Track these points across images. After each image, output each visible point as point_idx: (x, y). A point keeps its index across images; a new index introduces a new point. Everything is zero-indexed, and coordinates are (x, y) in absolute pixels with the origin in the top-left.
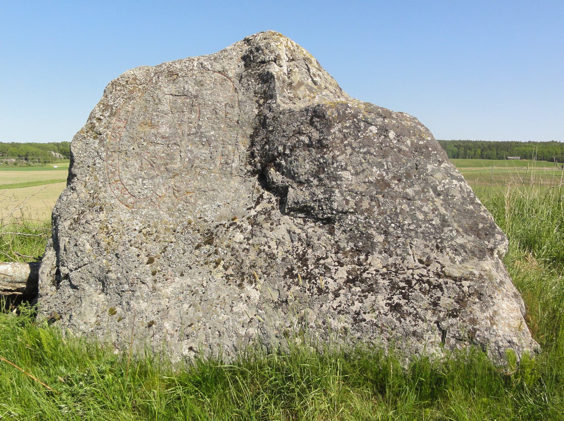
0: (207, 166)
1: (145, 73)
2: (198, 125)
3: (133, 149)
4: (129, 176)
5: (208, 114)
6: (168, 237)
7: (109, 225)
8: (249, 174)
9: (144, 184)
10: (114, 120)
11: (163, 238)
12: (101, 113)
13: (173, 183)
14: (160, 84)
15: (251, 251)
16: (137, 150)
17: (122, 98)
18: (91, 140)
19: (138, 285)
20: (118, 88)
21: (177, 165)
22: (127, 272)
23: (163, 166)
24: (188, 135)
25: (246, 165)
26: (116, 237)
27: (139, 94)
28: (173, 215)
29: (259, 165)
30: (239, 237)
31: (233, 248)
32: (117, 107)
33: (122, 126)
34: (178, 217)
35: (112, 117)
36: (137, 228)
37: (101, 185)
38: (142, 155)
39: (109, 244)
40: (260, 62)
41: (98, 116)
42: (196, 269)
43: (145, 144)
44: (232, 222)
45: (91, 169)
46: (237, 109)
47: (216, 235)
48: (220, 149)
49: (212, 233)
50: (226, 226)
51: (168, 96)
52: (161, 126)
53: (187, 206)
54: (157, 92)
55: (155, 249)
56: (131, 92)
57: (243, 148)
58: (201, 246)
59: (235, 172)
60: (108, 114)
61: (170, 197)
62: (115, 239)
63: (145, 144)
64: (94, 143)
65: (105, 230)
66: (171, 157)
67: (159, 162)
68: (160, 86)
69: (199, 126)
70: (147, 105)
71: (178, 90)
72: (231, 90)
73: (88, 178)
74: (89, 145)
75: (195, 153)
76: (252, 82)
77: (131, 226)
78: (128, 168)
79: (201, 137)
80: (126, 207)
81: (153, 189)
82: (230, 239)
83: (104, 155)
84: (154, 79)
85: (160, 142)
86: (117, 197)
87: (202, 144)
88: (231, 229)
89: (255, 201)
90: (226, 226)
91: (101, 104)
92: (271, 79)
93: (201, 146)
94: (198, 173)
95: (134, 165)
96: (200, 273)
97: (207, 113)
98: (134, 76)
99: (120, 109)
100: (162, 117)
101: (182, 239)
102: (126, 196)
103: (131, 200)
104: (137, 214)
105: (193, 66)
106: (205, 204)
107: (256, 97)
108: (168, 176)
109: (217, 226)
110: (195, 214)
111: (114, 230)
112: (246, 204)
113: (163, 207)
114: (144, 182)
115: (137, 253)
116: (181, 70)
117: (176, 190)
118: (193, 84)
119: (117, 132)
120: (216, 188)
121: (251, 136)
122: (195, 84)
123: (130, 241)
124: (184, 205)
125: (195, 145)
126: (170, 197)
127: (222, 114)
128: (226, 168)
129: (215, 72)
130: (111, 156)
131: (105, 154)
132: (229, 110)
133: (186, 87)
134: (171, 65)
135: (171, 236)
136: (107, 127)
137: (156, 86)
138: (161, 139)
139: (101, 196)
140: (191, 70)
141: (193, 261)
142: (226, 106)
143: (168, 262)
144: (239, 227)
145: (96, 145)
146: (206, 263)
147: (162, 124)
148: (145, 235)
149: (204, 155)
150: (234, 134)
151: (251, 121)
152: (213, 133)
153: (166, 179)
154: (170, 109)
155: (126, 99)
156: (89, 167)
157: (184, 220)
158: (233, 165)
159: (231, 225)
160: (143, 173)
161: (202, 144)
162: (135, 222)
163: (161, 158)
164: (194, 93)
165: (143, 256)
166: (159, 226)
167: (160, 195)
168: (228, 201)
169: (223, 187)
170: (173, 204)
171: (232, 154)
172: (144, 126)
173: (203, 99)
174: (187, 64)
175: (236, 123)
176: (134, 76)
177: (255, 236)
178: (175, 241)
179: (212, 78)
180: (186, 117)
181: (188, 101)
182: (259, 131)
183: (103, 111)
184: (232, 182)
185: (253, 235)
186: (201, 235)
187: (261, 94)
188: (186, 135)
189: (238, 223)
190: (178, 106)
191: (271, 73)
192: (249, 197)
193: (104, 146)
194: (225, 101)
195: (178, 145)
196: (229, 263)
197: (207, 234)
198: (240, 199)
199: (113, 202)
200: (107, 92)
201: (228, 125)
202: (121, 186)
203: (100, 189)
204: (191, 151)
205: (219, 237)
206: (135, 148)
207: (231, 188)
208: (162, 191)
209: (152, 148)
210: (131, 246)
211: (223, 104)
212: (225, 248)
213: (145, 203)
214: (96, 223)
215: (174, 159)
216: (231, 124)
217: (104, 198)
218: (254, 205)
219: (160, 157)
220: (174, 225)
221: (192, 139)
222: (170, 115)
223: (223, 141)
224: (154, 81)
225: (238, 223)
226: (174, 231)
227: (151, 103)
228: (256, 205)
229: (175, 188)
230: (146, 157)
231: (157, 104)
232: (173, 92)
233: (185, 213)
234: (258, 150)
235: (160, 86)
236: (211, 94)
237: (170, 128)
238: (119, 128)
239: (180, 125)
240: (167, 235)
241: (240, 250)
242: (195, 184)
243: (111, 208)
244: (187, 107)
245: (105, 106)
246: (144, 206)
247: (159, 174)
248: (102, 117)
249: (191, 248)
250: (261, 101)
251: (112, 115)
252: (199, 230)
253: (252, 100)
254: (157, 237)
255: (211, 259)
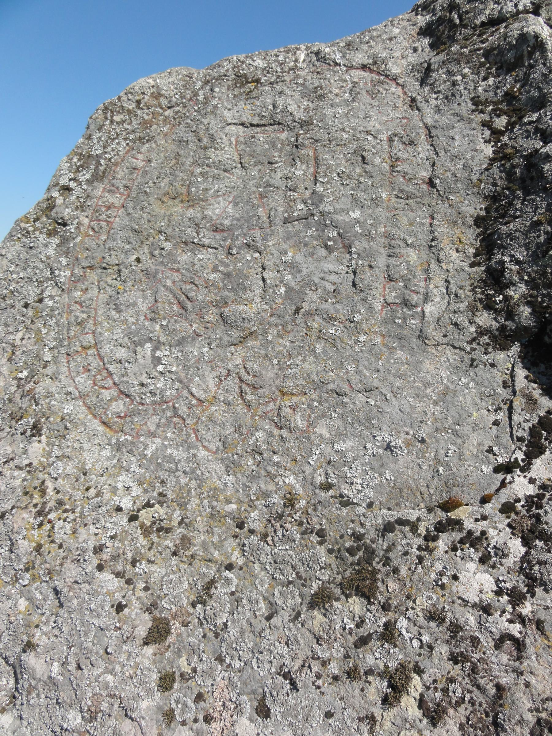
0: (343, 311)
1: (182, 83)
2: (314, 193)
3: (138, 260)
4: (118, 333)
5: (340, 165)
6: (219, 546)
7: (50, 485)
8: (486, 339)
9: (157, 361)
10: (99, 189)
11: (204, 546)
12: (72, 175)
13: (239, 361)
14: (214, 102)
15: (531, 650)
16: (148, 263)
17: (125, 139)
18: (42, 238)
19: (111, 722)
20: (117, 118)
21: (252, 307)
22: (79, 668)
23: (214, 310)
24: (286, 221)
25: (473, 309)
26: (63, 530)
27: (165, 129)
28: (238, 465)
29: (526, 311)
30: (477, 581)
31: (455, 628)
32: (110, 159)
33: (117, 203)
34: (253, 477)
35: (96, 184)
36: (126, 504)
37: (48, 357)
38: (160, 276)
39: (38, 548)
40: (483, 24)
41: (63, 181)
42: (314, 694)
43: (168, 246)
44: (441, 515)
45: (30, 312)
46: (424, 149)
47: (387, 561)
48: (382, 261)
49: (370, 553)
50: (422, 531)
51: (233, 127)
52: (212, 201)
53: (283, 440)
54: (206, 121)
55: (177, 585)
56: (146, 124)
57: (458, 256)
58: (330, 597)
59: (430, 330)
60: (88, 176)
61: (229, 404)
62: (58, 537)
63: (168, 246)
64: (46, 246)
65: (37, 499)
66: (237, 283)
67: (201, 296)
68: (216, 107)
69: (317, 198)
70: (182, 153)
71: (258, 111)
72: (400, 103)
73: (20, 335)
74: (34, 252)
75: (305, 272)
76: (464, 76)
77: (107, 495)
78: (119, 311)
79: (322, 226)
80: (101, 428)
81: (182, 375)
82: (443, 587)
83: (64, 275)
84: (201, 92)
85: (206, 241)
86: (83, 396)
87: (327, 247)
88: (442, 544)
89: (521, 439)
90: (422, 531)
91: (76, 154)
92: (531, 54)
93: (323, 252)
94: (315, 333)
95: (134, 304)
96: (329, 715)
97: (337, 161)
98: (155, 90)
99: (116, 164)
100: (217, 177)
101: (263, 559)
102: (106, 394)
103: (119, 406)
104: (130, 452)
105: (296, 61)
106: (340, 436)
107: (482, 112)
108: (226, 339)
109: (388, 528)
110: (308, 470)
111: (60, 503)
112: (490, 450)
113: (208, 436)
114: (158, 353)
115: (118, 596)
116: (267, 70)
117: (248, 385)
118: (297, 96)
119: (103, 217)
120: (376, 383)
121: (479, 221)
122: (304, 95)
123: (98, 549)
124: (271, 435)
125: (304, 250)
126: (229, 404)
127: (379, 162)
128: (404, 319)
129: (352, 68)
130: (83, 278)
131: (68, 273)
132: (398, 148)
133: (280, 102)
134: (243, 62)
135: (231, 544)
136: (82, 207)
137: (206, 108)
138: (210, 234)
139: (40, 389)
140: (291, 69)
141: (301, 656)
142: (390, 140)
143: (217, 642)
144: (474, 540)
145: (51, 251)
146: (352, 674)
147: (216, 195)
148: (146, 531)
149: (333, 278)
150: (421, 217)
151: (474, 177)
152: (356, 214)
153: (220, 346)
154: (236, 158)
155: (134, 141)
156: (26, 306)
157: (271, 487)
158: (428, 308)
159: (440, 527)
160: (158, 327)
161: (327, 247)
162: (124, 479)
163: (208, 285)
164: (300, 115)
165: (134, 610)
166: (194, 503)
167: (201, 395)
168: (423, 433)
169: (399, 382)
170: (238, 429)
171: (420, 274)
172: (171, 202)
173: (327, 128)
174: (281, 58)
175: (425, 187)
176: (155, 90)
177: (544, 584)
178: (241, 561)
179: (345, 81)
180: (279, 174)
181: (283, 136)
182: (510, 204)
183: (78, 171)
184: (428, 366)
185: (533, 582)
186: (330, 551)
187: (495, 103)
188: (278, 221)
189: (469, 524)
190: (258, 149)
191: (536, 36)
192: (496, 423)
193: (67, 254)
194: (387, 130)
195: (257, 250)
196: (445, 691)
197: (351, 551)
198: (465, 429)
199: (68, 408)
200: (92, 127)
201: (401, 191)
202: (95, 363)
203: (45, 367)
204: (293, 267)
205: (396, 571)
206: (143, 258)
207: (427, 385)
208: (206, 384)
209: (185, 257)
210: (100, 568)
211: (384, 137)
212: (421, 619)
213: (156, 419)
214: (16, 473)
215: (245, 290)
216: (410, 189)
217: (49, 395)
218: (520, 455)
219: (206, 281)
220: (240, 502)
221: (297, 233)
222: (238, 172)
223: (388, 236)
224: (201, 98)
225: (469, 524)
226: (240, 526)
227: (191, 146)
228: (530, 457)
229: (245, 377)
230: (169, 283)
231: (205, 148)
232: (247, 118)
233: (277, 465)
234: (518, 262)
235: (216, 107)
236: (346, 115)
237: (236, 204)
238: (109, 208)
239: (262, 196)
240: (216, 539)
241: (487, 642)
242: (306, 366)
243: (61, 428)
244: (281, 150)
245: (86, 159)
246: (153, 428)
247: (201, 330)
248: (72, 184)
249: (295, 599)
250: (501, 122)
251: (97, 177)
252: (321, 534)
253: (470, 121)
254: (185, 541)
255: (370, 660)
